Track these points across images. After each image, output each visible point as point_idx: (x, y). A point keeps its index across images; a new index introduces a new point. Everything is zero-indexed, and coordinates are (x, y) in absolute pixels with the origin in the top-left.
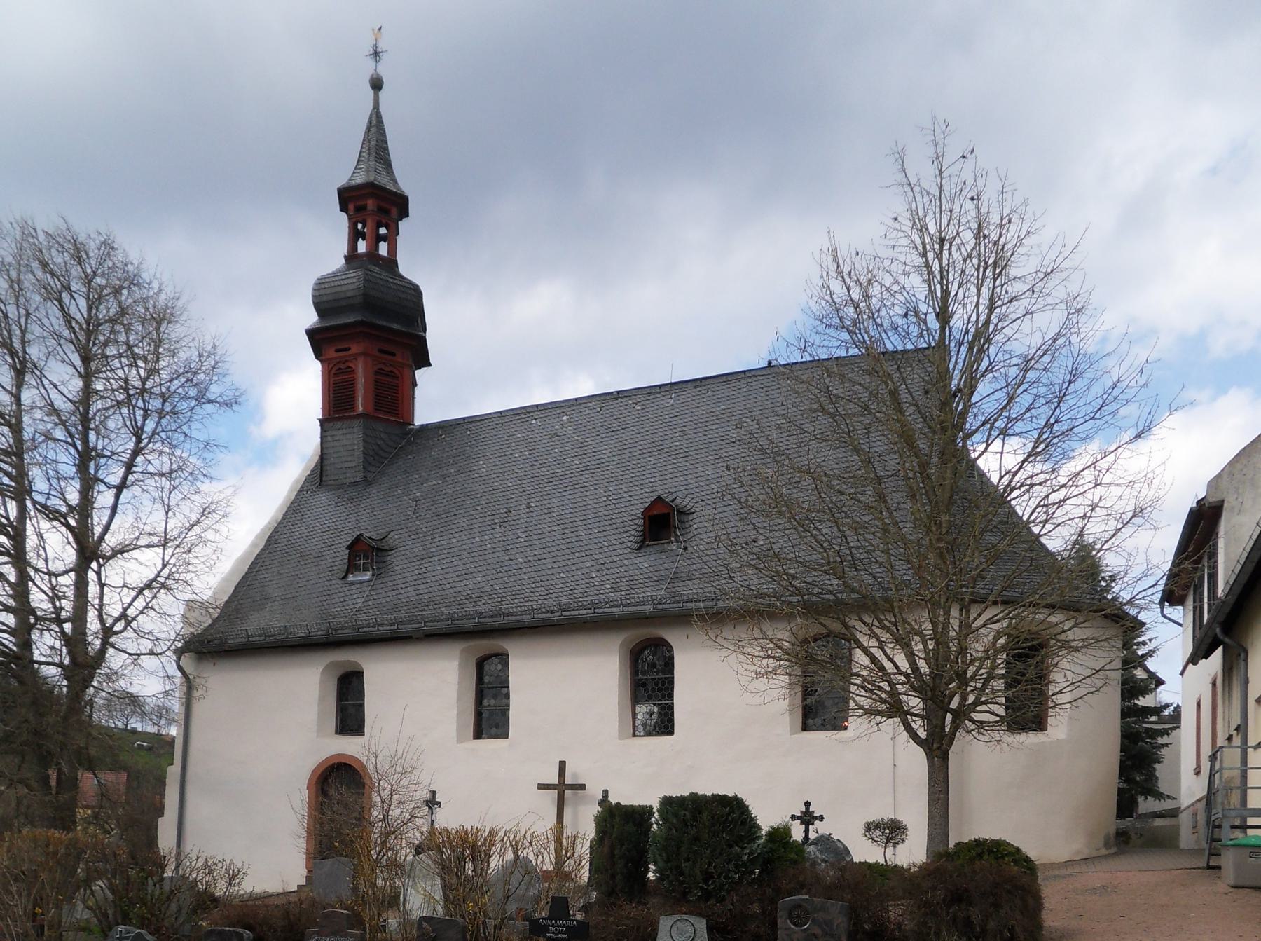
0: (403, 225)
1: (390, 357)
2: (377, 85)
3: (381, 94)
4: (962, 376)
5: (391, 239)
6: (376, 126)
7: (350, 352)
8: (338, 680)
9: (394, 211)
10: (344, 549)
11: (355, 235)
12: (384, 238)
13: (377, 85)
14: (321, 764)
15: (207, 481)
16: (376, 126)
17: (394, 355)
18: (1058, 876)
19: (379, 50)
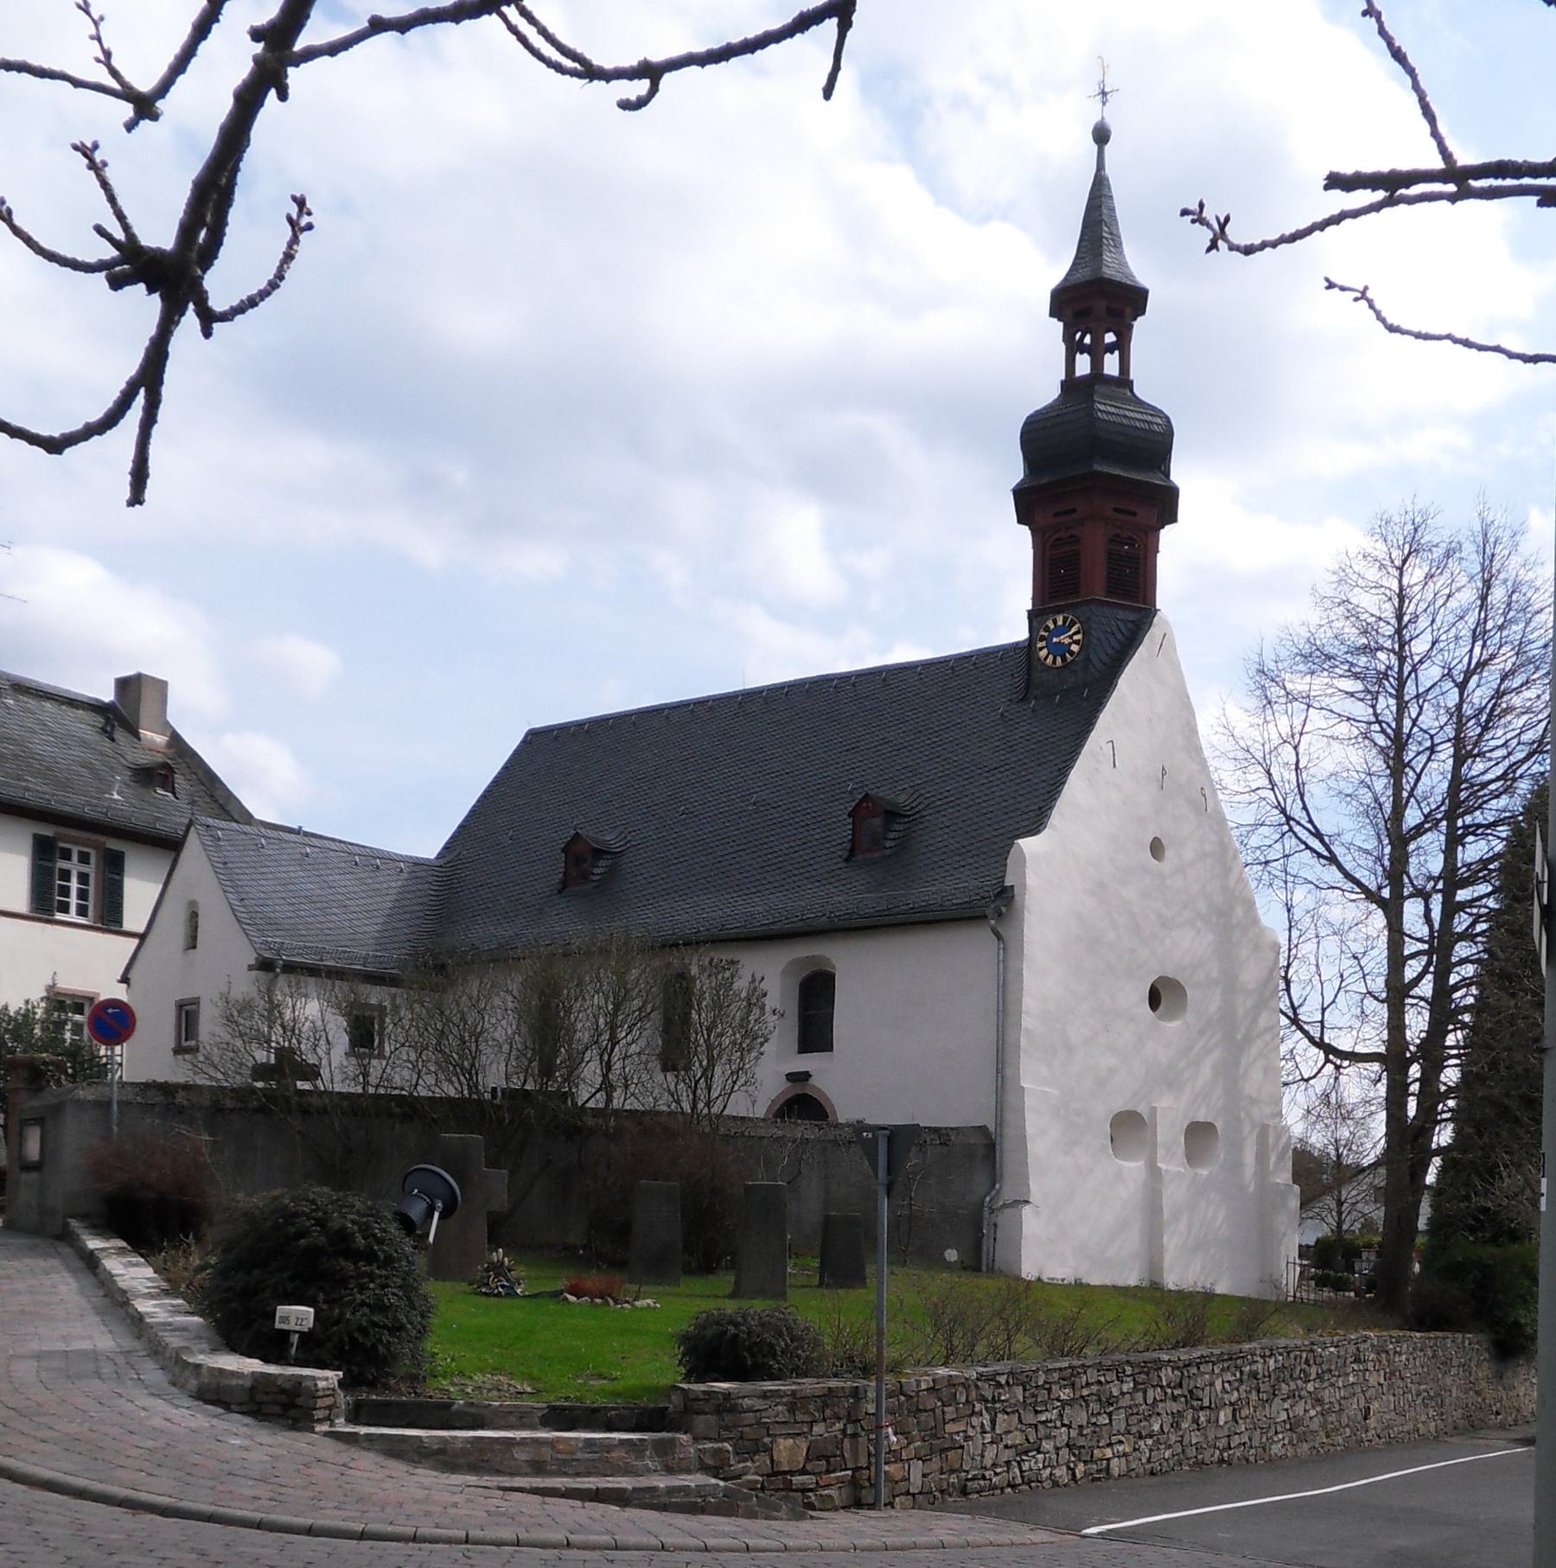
0: (1139, 324)
1: (1130, 518)
2: (1101, 136)
3: (1108, 148)
4: (1489, 701)
5: (1122, 346)
6: (1099, 195)
7: (1075, 516)
8: (801, 985)
9: (1128, 311)
10: (845, 817)
11: (1073, 348)
12: (1110, 348)
13: (1101, 136)
14: (824, 1095)
15: (1512, 568)
16: (1099, 195)
17: (1134, 514)
18: (568, 1453)
19: (1107, 90)
